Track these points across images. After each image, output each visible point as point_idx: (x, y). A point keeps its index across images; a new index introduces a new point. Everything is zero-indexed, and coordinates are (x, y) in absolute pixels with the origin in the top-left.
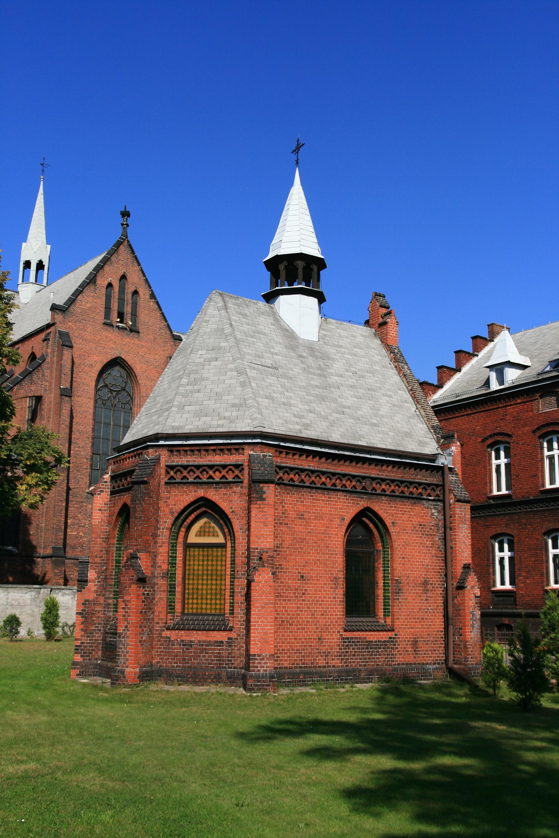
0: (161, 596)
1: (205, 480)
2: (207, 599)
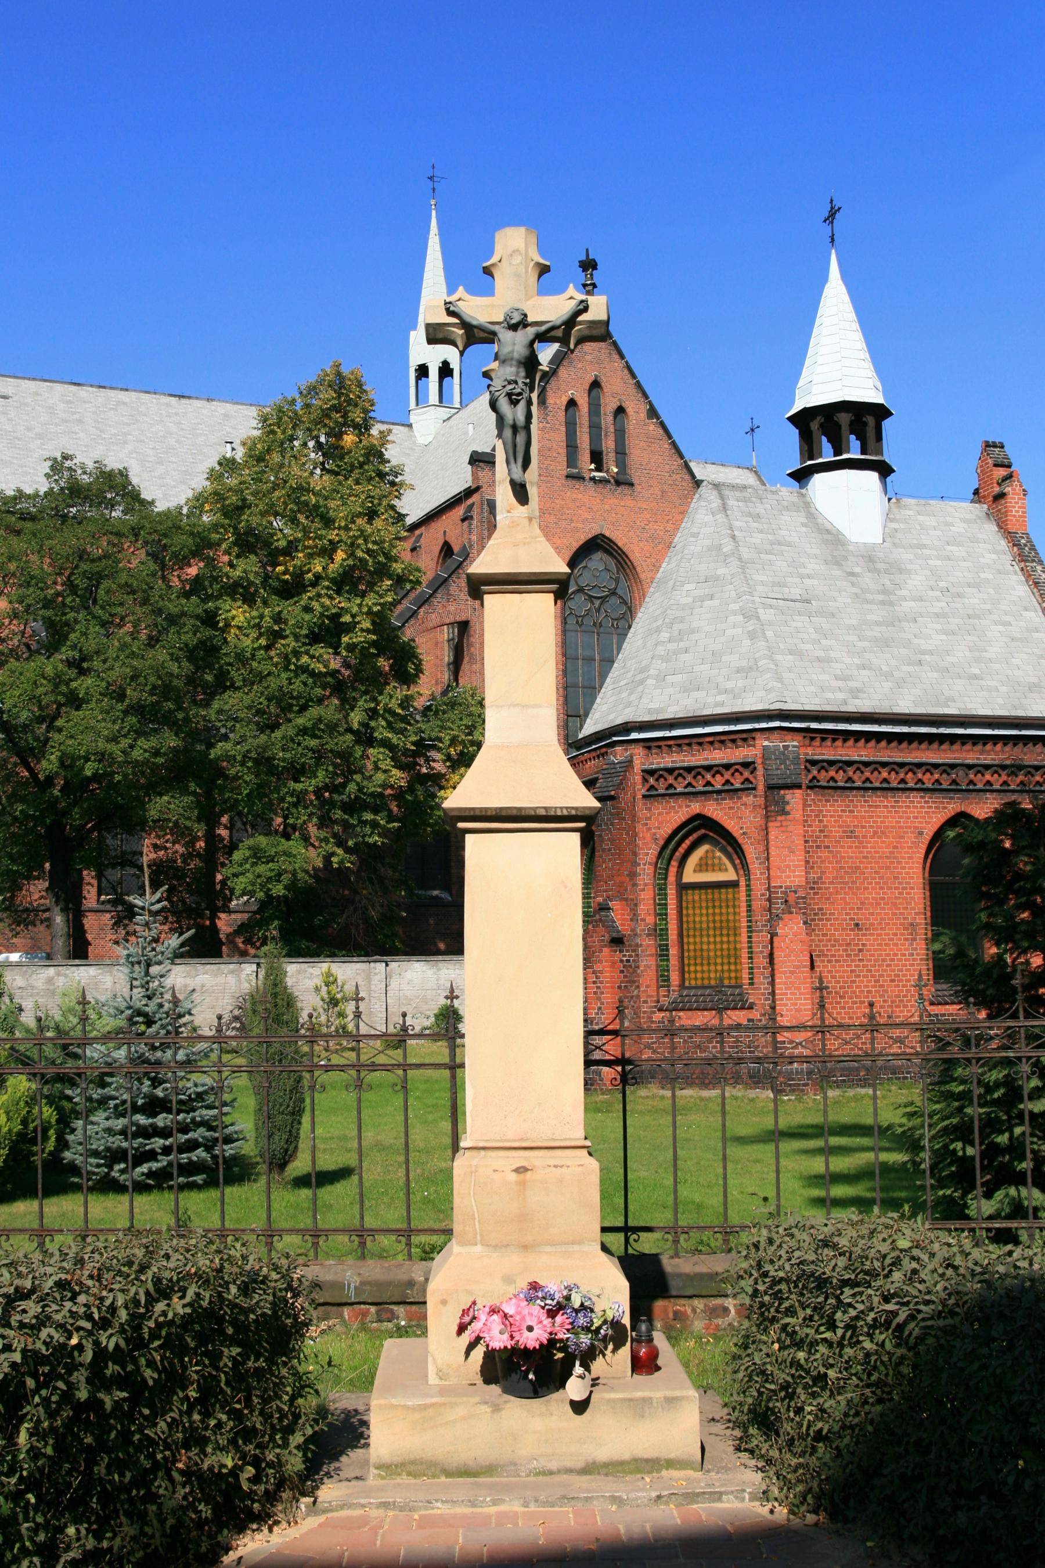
0: (648, 963)
1: (700, 788)
2: (716, 964)
